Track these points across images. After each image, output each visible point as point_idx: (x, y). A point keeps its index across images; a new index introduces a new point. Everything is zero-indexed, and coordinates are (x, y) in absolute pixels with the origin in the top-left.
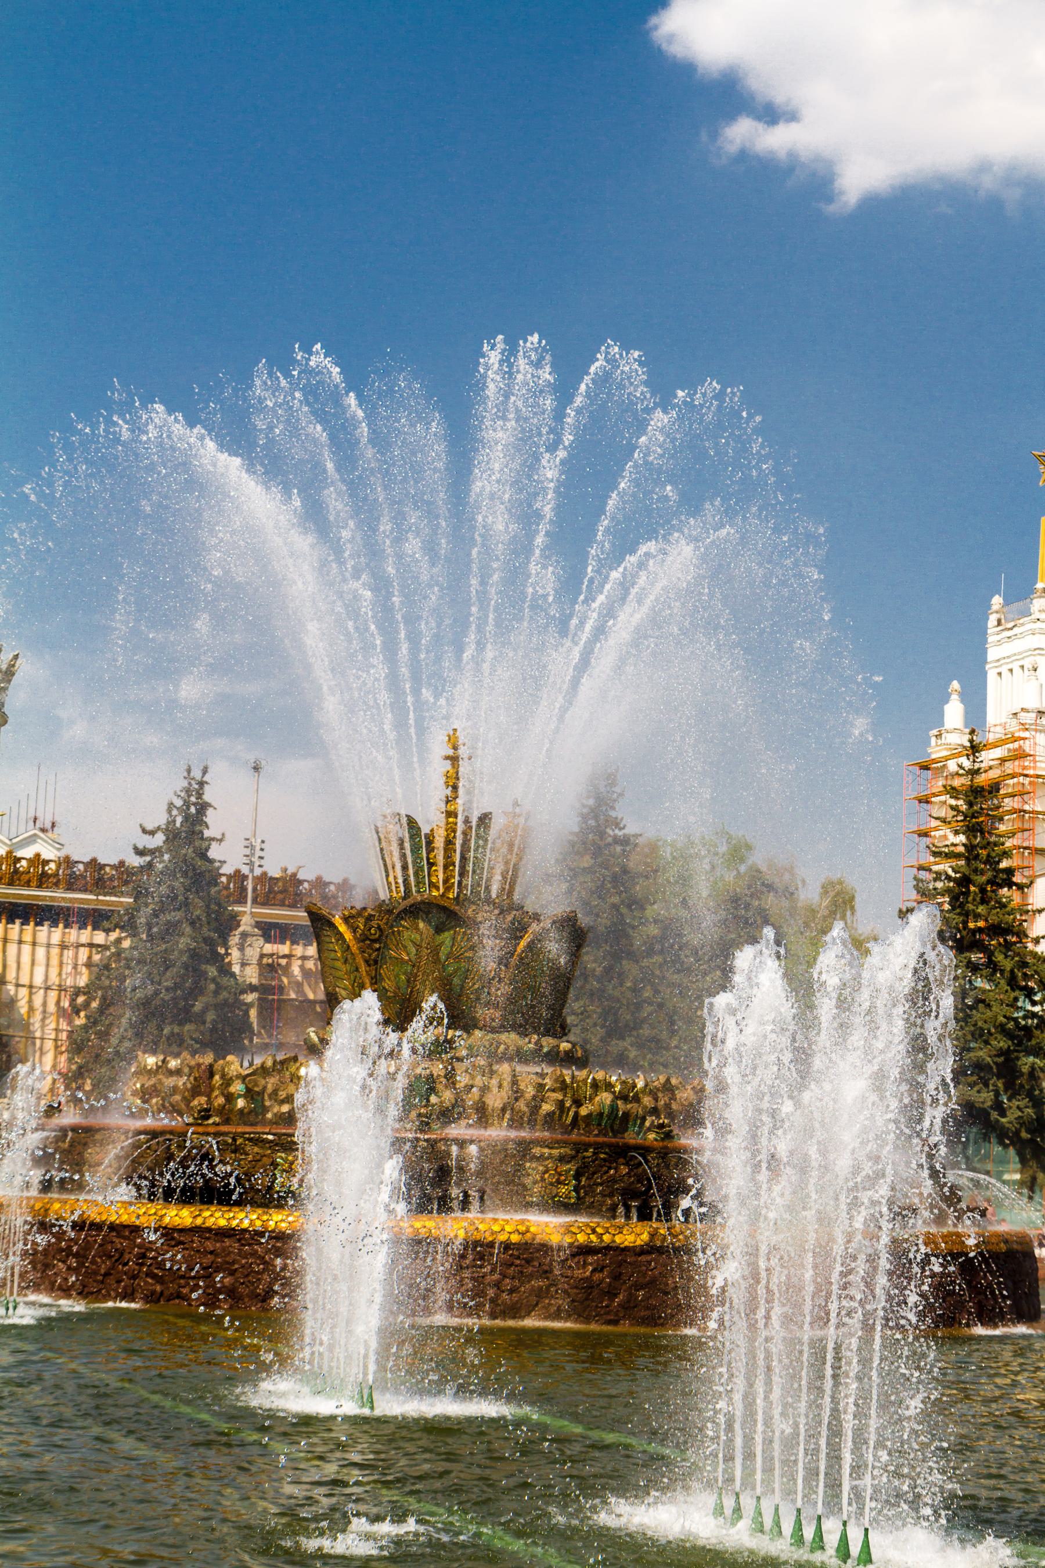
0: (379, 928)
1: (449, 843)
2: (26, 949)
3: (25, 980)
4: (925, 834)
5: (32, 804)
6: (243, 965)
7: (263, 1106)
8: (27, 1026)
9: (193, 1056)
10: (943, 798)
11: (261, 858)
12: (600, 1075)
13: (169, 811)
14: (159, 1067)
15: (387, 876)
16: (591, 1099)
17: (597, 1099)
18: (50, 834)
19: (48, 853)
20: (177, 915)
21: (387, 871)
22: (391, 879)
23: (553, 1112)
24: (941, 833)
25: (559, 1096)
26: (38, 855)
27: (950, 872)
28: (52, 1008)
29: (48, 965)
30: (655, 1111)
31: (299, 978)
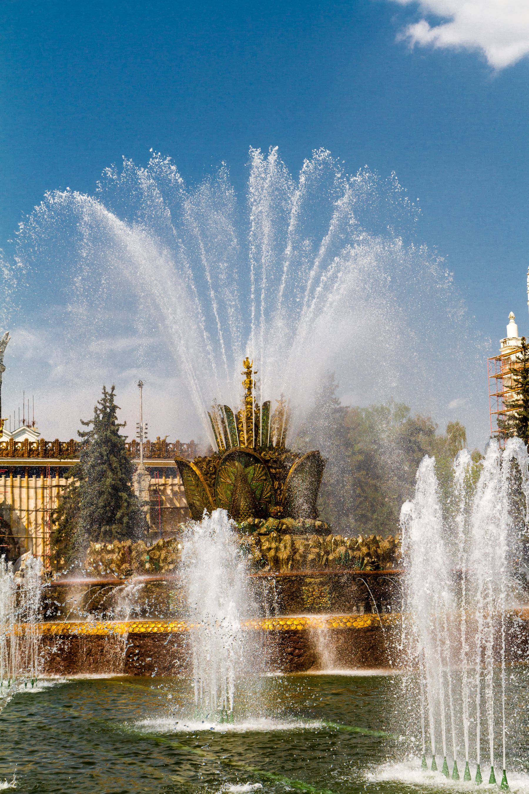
0: (214, 467)
1: (248, 418)
2: (24, 490)
3: (24, 507)
4: (501, 396)
5: (21, 412)
6: (141, 491)
7: (159, 566)
8: (27, 531)
9: (120, 542)
10: (509, 375)
11: (146, 433)
12: (338, 538)
13: (96, 411)
14: (102, 549)
15: (217, 438)
16: (334, 551)
17: (338, 550)
18: (32, 428)
19: (32, 439)
20: (105, 467)
21: (216, 436)
22: (219, 440)
23: (314, 559)
24: (510, 394)
25: (317, 550)
26: (27, 440)
27: (516, 415)
28: (40, 521)
29: (36, 499)
30: (368, 555)
31: (171, 496)
